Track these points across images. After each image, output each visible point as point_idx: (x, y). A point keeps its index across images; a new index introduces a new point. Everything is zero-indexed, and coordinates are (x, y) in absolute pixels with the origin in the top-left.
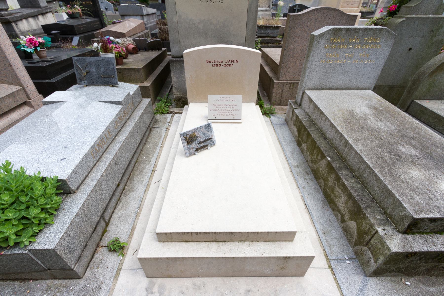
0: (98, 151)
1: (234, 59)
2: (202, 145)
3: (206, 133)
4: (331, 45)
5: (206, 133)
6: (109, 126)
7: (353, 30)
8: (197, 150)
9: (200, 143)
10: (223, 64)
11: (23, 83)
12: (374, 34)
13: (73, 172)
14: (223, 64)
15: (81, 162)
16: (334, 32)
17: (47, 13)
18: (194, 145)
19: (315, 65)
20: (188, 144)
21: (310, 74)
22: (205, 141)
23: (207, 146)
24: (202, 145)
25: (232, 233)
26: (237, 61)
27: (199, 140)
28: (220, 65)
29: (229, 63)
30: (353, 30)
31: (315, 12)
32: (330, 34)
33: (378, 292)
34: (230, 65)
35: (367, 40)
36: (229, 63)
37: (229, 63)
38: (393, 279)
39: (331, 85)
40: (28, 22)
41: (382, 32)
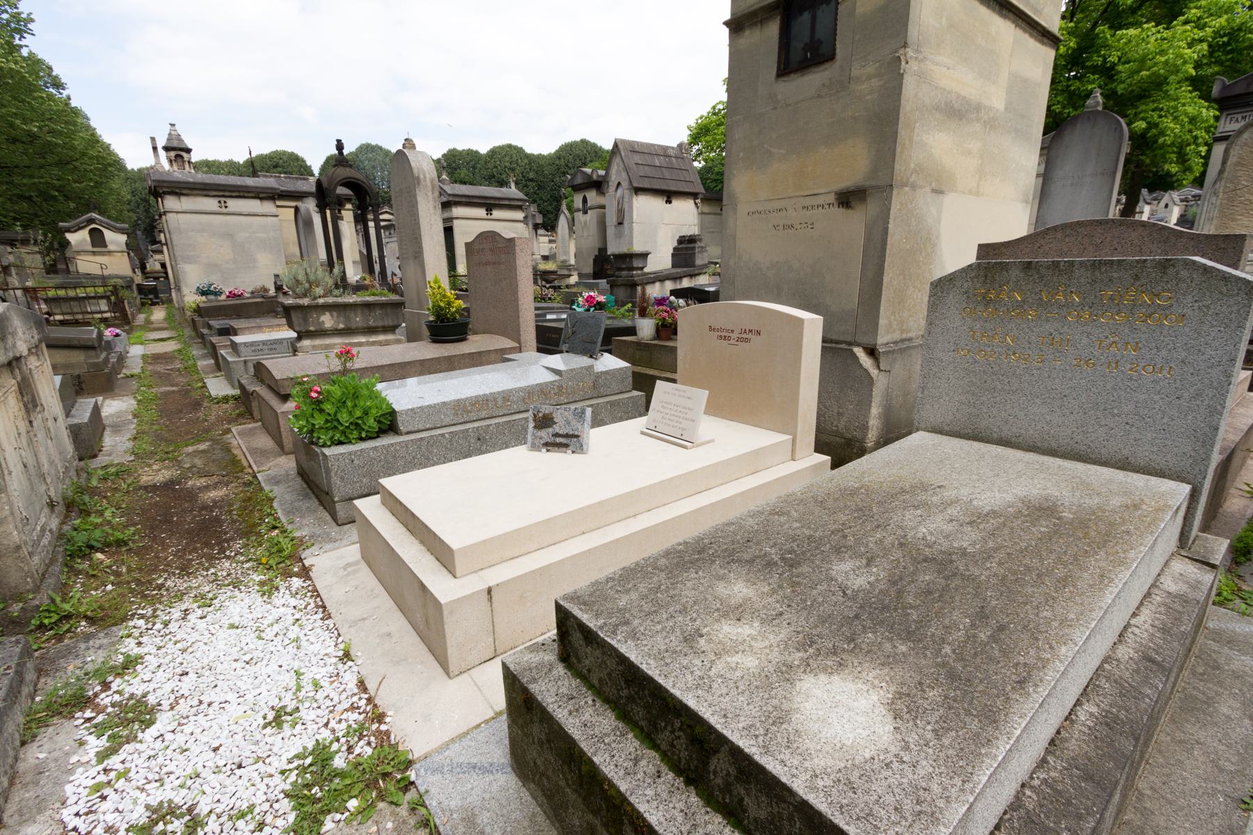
0: (468, 412)
1: (754, 328)
2: (558, 440)
3: (574, 422)
4: (979, 308)
5: (574, 422)
6: (510, 391)
7: (1048, 268)
8: (546, 444)
9: (556, 435)
10: (734, 336)
11: (522, 340)
12: (1137, 278)
13: (412, 410)
14: (734, 336)
15: (430, 406)
16: (982, 273)
17: (699, 274)
18: (546, 434)
19: (941, 361)
20: (535, 427)
21: (930, 385)
22: (567, 436)
23: (566, 446)
24: (558, 440)
25: (413, 515)
26: (759, 333)
27: (557, 429)
28: (729, 338)
29: (745, 336)
30: (1048, 268)
31: (1059, 235)
32: (972, 279)
33: (487, 796)
34: (747, 340)
35: (1112, 298)
36: (746, 335)
37: (745, 336)
38: (541, 818)
39: (1006, 432)
40: (662, 287)
41: (1171, 271)
